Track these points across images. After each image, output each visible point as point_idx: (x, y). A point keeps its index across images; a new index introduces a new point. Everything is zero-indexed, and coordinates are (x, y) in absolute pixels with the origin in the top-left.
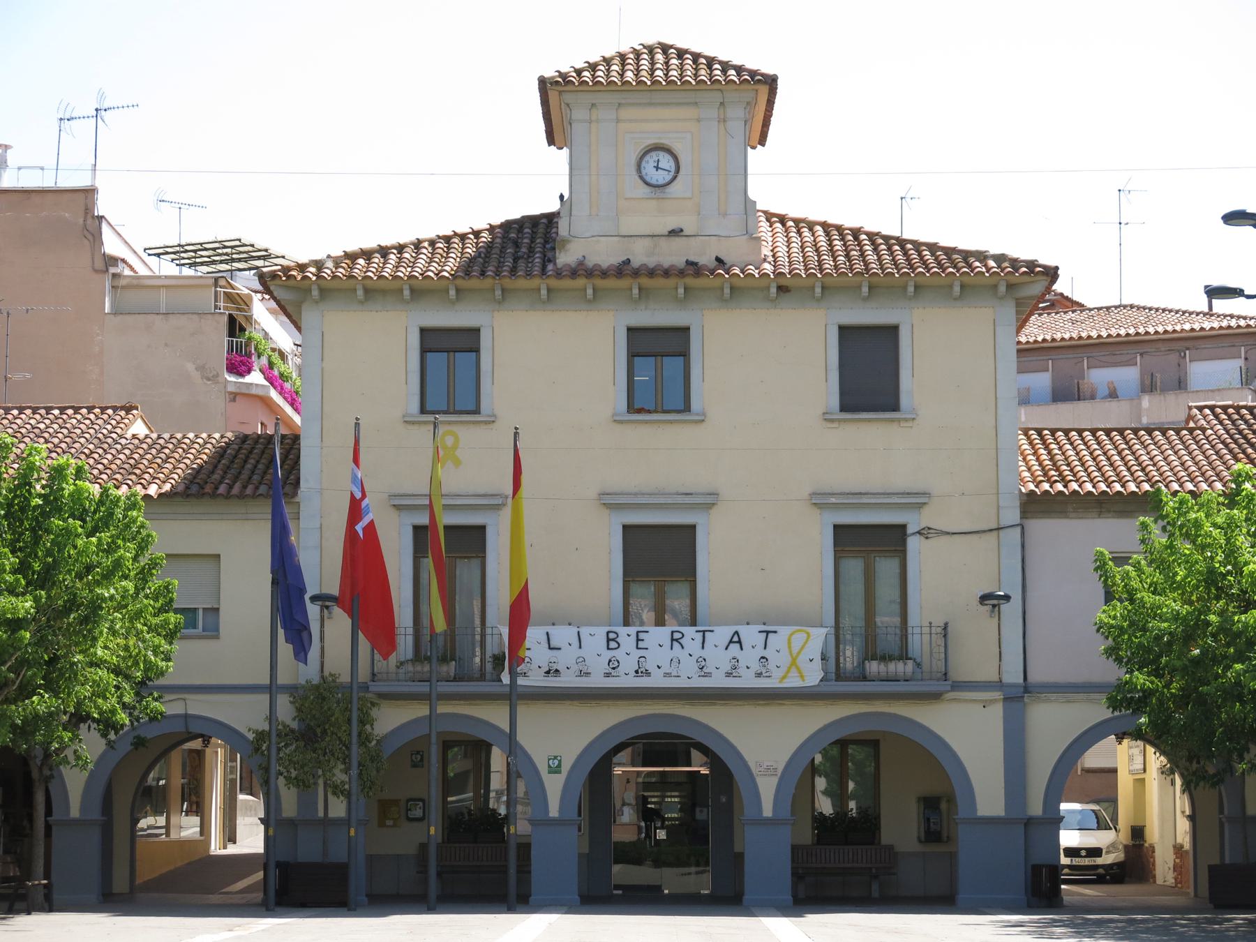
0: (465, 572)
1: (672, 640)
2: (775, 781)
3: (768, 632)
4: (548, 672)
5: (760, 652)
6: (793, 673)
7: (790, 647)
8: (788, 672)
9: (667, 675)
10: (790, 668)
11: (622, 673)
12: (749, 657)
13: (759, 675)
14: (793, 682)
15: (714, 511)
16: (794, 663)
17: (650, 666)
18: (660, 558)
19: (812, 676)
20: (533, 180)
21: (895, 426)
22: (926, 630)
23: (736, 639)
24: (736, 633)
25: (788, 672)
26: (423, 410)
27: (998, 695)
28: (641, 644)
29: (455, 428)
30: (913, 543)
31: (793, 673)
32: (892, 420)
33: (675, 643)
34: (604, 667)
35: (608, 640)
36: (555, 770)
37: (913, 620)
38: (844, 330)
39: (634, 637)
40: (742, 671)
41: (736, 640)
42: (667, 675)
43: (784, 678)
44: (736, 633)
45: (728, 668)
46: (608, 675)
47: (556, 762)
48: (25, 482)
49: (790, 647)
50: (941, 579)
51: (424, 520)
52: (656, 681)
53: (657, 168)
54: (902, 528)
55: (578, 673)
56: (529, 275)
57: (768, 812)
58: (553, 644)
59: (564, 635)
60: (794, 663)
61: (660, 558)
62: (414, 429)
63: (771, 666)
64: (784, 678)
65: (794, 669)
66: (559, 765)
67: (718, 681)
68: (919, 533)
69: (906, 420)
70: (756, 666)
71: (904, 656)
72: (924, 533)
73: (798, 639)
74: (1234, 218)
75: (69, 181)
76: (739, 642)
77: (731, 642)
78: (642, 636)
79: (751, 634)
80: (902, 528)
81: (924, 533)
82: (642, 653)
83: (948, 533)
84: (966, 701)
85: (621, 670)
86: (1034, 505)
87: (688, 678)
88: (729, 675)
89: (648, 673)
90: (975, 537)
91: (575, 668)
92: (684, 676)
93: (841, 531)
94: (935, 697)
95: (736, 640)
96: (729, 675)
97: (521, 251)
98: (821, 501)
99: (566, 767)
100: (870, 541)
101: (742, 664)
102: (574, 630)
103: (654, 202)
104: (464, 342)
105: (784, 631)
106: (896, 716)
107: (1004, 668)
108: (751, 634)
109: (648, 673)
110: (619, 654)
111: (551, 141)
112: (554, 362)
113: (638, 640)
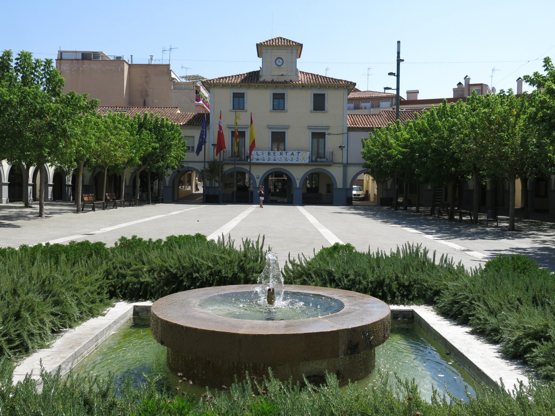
12: (295, 157)
14: (303, 162)
18: (278, 138)
19: (307, 161)
20: (254, 64)
30: (327, 136)
37: (326, 151)
38: (314, 95)
41: (293, 154)
57: (298, 186)
59: (260, 152)
61: (278, 138)
74: (399, 42)
79: (295, 153)
94: (330, 165)
95: (293, 154)
100: (319, 136)
104: (242, 96)
105: (302, 152)
108: (295, 153)
111: (258, 56)
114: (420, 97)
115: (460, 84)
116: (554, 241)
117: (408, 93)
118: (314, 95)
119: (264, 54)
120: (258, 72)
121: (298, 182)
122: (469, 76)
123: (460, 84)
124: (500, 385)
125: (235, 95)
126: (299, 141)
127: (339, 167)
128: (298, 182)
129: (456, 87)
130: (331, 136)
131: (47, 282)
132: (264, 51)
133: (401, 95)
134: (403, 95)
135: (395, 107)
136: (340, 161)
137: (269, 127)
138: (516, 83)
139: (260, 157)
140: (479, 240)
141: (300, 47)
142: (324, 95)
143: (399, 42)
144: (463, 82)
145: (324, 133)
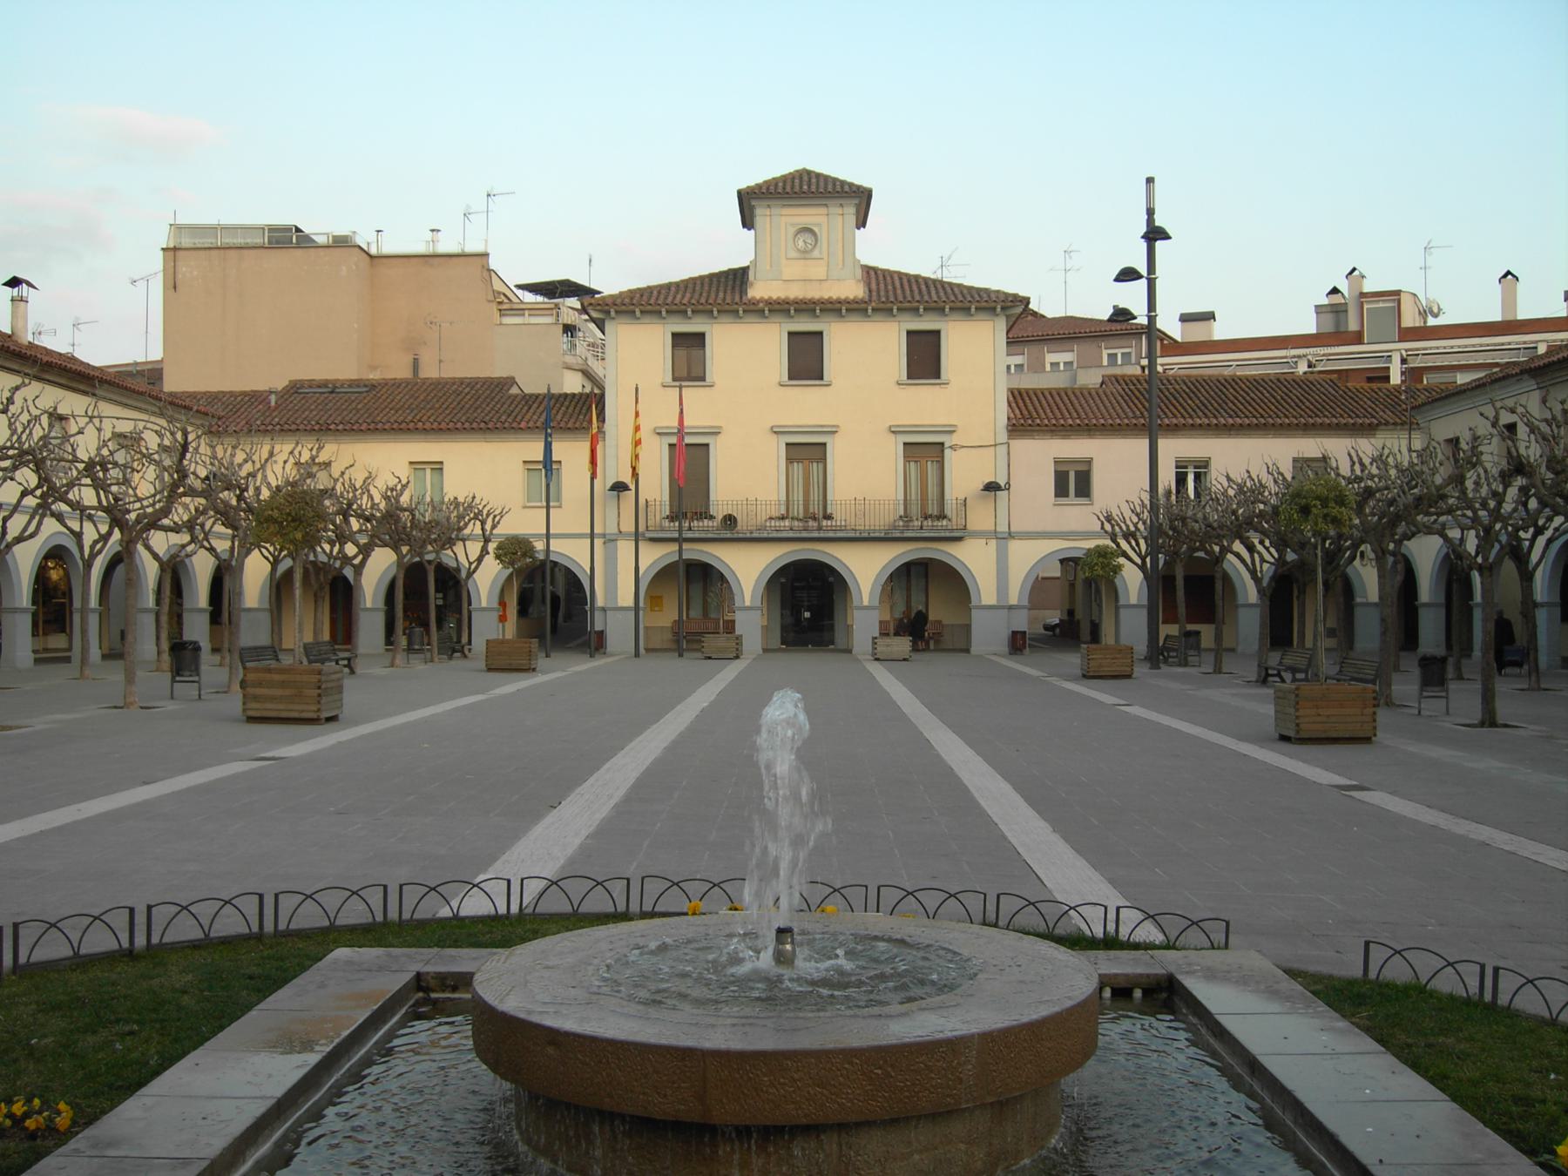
0: (1342, 315)
20: (724, 245)
26: (674, 379)
30: (947, 452)
37: (947, 496)
38: (909, 333)
50: (964, 475)
51: (674, 440)
54: (942, 444)
56: (1454, 442)
71: (942, 516)
74: (1150, 181)
75: (472, 247)
80: (942, 444)
86: (385, 887)
94: (959, 539)
97: (725, 293)
104: (699, 339)
111: (744, 226)
112: (746, 353)
114: (1221, 331)
115: (1335, 291)
116: (4, 728)
117: (1185, 318)
118: (909, 333)
119: (759, 221)
120: (744, 271)
122: (1361, 268)
123: (1335, 291)
125: (678, 339)
129: (1325, 301)
131: (643, 994)
132: (758, 211)
133: (1161, 324)
134: (1169, 324)
135: (1145, 362)
137: (894, 431)
138: (1498, 288)
140: (682, 728)
142: (819, 334)
143: (1150, 181)
144: (1344, 287)
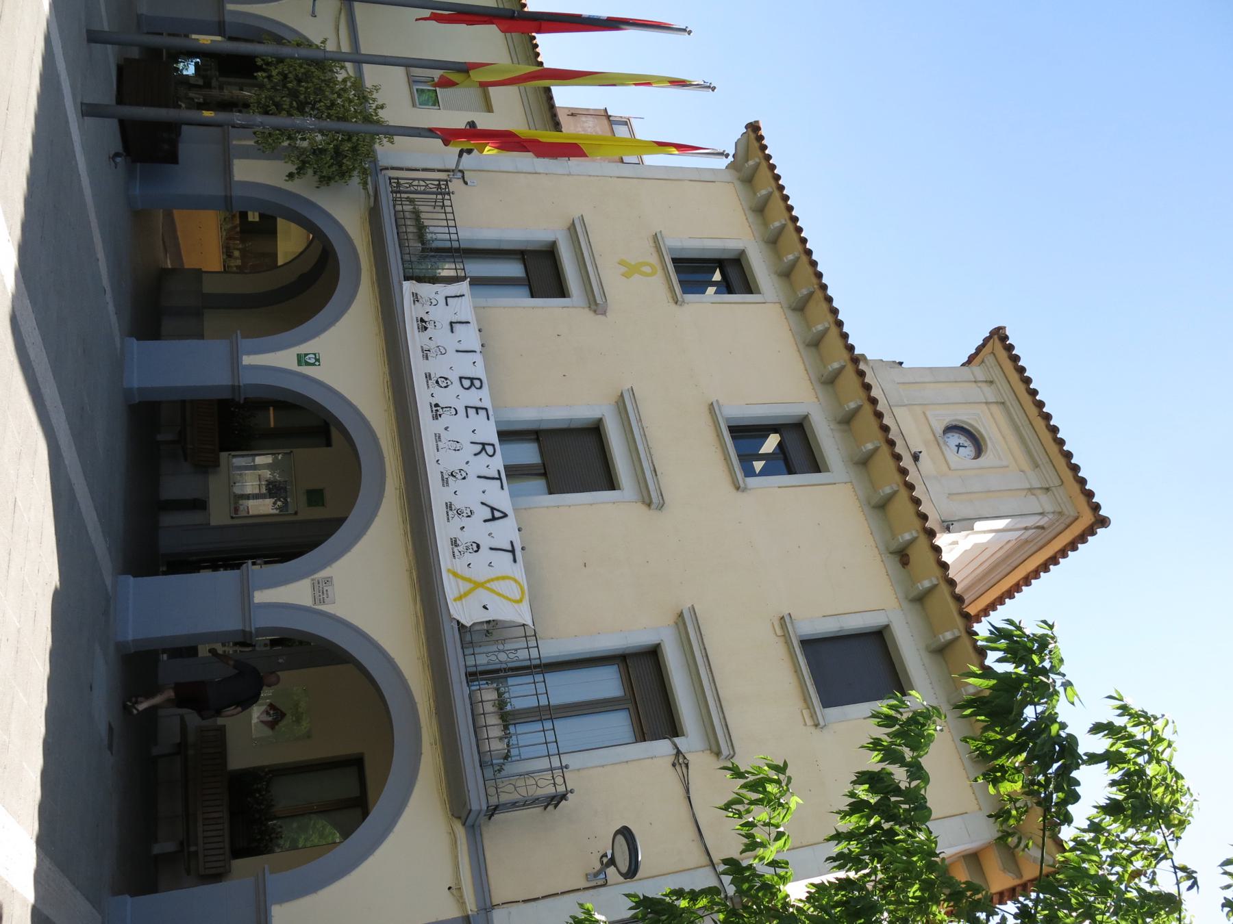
1: (483, 444)
2: (307, 601)
3: (513, 551)
4: (422, 320)
5: (485, 543)
6: (464, 587)
7: (497, 579)
8: (464, 578)
9: (438, 438)
10: (469, 580)
11: (432, 390)
12: (476, 530)
13: (454, 543)
14: (451, 588)
15: (644, 508)
16: (478, 585)
17: (446, 419)
18: (570, 457)
19: (466, 611)
21: (800, 704)
22: (556, 762)
23: (497, 514)
24: (505, 515)
25: (464, 578)
27: (471, 906)
28: (472, 412)
29: (660, 272)
30: (663, 747)
31: (464, 587)
32: (806, 699)
33: (479, 447)
34: (436, 374)
35: (472, 379)
36: (301, 360)
39: (479, 404)
40: (457, 522)
41: (496, 515)
42: (438, 438)
43: (455, 575)
44: (505, 515)
45: (457, 505)
46: (428, 376)
47: (313, 361)
48: (514, 472)
49: (497, 579)
52: (428, 427)
53: (959, 446)
55: (426, 348)
57: (260, 597)
58: (457, 327)
59: (469, 337)
60: (478, 585)
61: (570, 457)
62: (649, 246)
63: (469, 557)
64: (455, 575)
65: (471, 585)
66: (308, 364)
67: (439, 496)
68: (679, 752)
69: (813, 715)
70: (465, 538)
72: (680, 761)
73: (512, 590)
76: (494, 519)
77: (493, 509)
78: (482, 413)
79: (505, 532)
81: (680, 761)
82: (462, 411)
83: (688, 791)
84: (455, 858)
85: (437, 390)
87: (436, 461)
88: (449, 506)
89: (436, 416)
90: (691, 832)
91: (432, 345)
92: (438, 456)
93: (653, 654)
95: (496, 515)
96: (449, 506)
98: (685, 624)
99: (305, 370)
100: (647, 691)
101: (465, 521)
102: (478, 348)
103: (931, 437)
105: (518, 571)
106: (418, 754)
107: (514, 909)
108: (505, 532)
109: (436, 416)
110: (456, 387)
113: (477, 409)
121: (284, 359)
124: (1018, 533)
126: (572, 580)
127: (455, 890)
128: (284, 359)
130: (671, 778)
136: (502, 886)
139: (440, 335)
141: (1087, 518)
145: (672, 728)
